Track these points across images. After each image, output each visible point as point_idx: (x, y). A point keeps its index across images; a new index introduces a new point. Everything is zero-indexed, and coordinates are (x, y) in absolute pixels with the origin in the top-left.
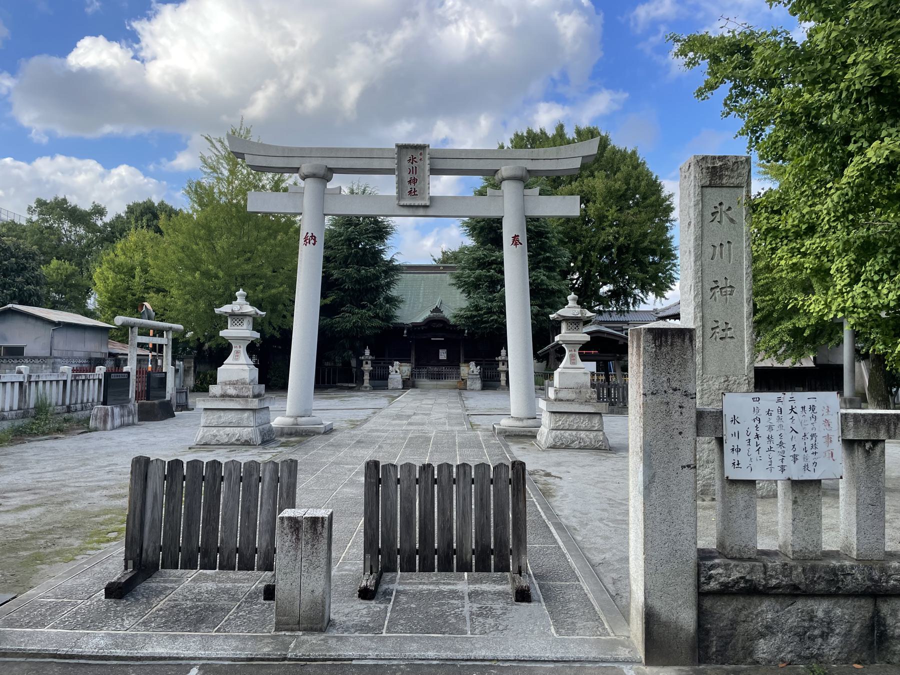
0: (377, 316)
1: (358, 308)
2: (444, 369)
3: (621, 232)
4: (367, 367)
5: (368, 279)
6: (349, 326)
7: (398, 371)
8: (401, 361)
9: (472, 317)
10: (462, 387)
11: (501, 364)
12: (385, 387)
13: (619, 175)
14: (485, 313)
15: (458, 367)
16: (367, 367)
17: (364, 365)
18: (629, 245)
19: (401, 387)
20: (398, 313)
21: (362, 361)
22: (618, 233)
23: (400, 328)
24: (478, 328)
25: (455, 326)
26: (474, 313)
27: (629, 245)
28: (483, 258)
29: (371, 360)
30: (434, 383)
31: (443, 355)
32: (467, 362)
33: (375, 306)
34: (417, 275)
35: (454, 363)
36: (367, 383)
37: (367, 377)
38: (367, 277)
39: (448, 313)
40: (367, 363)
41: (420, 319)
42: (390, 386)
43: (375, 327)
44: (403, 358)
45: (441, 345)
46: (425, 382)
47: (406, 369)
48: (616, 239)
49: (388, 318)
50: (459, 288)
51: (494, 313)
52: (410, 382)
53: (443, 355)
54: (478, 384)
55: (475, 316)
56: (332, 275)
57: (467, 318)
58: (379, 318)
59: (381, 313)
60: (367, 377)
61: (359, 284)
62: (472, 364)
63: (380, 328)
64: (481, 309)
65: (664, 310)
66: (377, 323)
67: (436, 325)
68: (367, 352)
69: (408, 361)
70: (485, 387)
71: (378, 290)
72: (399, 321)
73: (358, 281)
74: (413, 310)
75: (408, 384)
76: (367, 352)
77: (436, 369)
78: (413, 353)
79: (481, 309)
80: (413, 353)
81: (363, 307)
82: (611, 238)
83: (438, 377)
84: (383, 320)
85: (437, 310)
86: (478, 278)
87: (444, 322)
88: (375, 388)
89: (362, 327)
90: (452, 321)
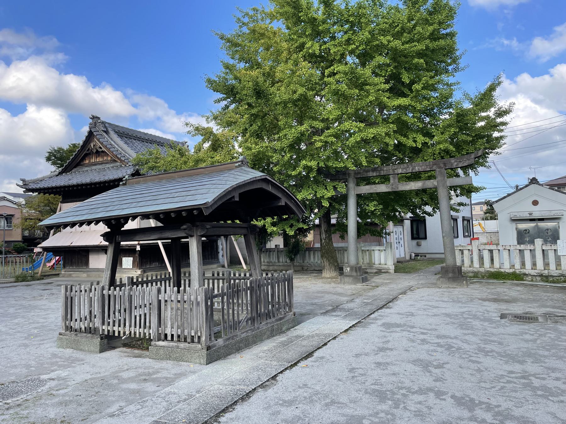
65: (34, 182)
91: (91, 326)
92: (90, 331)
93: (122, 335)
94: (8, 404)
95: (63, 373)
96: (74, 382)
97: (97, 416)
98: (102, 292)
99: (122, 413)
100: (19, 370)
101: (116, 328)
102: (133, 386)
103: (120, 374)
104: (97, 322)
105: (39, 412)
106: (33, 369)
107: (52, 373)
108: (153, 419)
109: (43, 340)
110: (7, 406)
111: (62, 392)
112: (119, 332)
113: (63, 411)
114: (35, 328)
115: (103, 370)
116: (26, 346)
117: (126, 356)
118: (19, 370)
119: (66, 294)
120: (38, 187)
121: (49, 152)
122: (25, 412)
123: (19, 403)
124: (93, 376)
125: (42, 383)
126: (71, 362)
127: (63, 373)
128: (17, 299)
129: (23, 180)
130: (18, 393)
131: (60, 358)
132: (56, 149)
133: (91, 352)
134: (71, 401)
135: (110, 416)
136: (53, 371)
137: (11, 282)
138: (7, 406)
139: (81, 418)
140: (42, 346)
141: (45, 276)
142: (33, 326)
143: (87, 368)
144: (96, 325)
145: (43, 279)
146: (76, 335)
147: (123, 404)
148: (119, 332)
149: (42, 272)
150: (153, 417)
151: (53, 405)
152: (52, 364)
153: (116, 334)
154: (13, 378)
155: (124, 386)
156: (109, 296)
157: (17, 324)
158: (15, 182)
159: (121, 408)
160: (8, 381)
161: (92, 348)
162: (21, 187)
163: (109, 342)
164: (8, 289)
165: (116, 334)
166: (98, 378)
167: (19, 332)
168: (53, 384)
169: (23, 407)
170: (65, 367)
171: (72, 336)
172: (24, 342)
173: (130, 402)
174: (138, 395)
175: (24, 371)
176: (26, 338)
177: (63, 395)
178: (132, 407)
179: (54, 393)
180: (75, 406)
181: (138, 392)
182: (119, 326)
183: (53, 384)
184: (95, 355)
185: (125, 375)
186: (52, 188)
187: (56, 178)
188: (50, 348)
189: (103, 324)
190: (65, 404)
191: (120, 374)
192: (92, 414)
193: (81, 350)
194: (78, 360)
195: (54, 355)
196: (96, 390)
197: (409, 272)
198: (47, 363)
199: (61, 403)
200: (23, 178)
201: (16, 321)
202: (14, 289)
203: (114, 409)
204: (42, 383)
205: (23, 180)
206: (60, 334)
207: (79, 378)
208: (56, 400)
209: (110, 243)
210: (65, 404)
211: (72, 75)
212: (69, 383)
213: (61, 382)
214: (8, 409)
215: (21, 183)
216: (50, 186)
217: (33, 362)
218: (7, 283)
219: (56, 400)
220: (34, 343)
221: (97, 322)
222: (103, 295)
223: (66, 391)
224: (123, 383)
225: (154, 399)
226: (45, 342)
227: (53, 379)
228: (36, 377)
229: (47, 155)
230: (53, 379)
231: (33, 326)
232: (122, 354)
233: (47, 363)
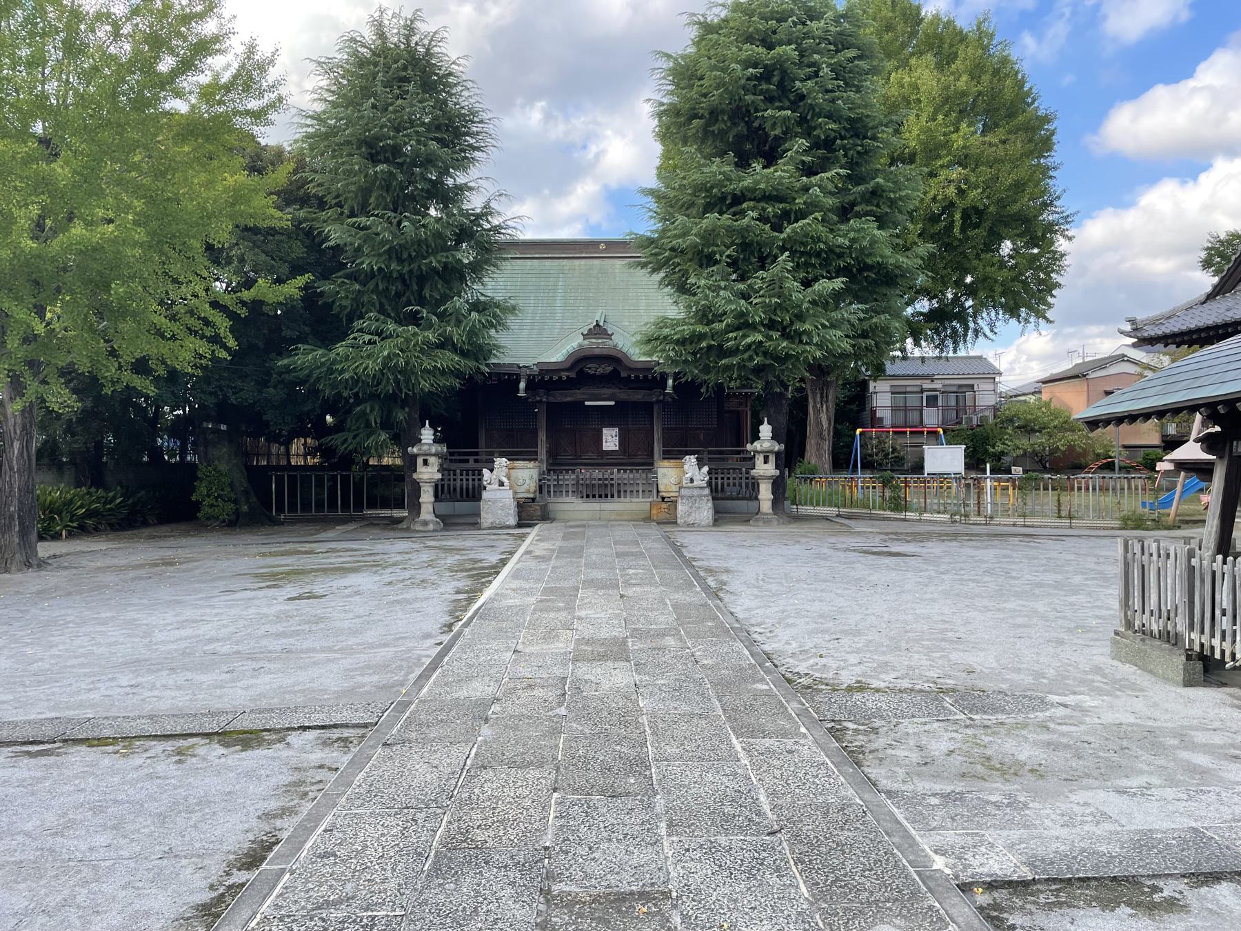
0: (445, 343)
1: (399, 322)
2: (616, 474)
3: (973, 179)
4: (428, 473)
5: (422, 247)
6: (373, 366)
7: (506, 481)
8: (512, 456)
9: (696, 338)
10: (663, 516)
11: (759, 460)
12: (472, 522)
13: (958, 65)
14: (731, 328)
15: (648, 464)
16: (428, 473)
17: (420, 467)
18: (986, 207)
19: (512, 521)
20: (498, 337)
21: (415, 456)
22: (967, 181)
23: (506, 380)
24: (707, 370)
25: (647, 369)
26: (700, 329)
27: (986, 207)
28: (720, 184)
29: (778, 454)
30: (594, 506)
31: (610, 440)
32: (674, 452)
33: (441, 317)
34: (548, 263)
35: (637, 457)
36: (427, 513)
37: (427, 497)
38: (419, 242)
39: (629, 342)
40: (425, 462)
41: (557, 354)
42: (487, 518)
43: (443, 372)
44: (519, 449)
45: (608, 417)
46: (571, 506)
47: (526, 475)
48: (961, 192)
49: (477, 351)
50: (654, 270)
51: (753, 327)
52: (536, 509)
53: (610, 440)
54: (705, 511)
55: (702, 337)
56: (327, 239)
57: (682, 342)
58: (454, 349)
59: (457, 334)
60: (427, 497)
61: (400, 261)
62: (691, 460)
63: (458, 374)
64: (719, 317)
65: (1155, 322)
66: (447, 359)
67: (596, 369)
68: (427, 435)
69: (531, 456)
70: (721, 516)
71: (454, 276)
72: (507, 360)
73: (394, 253)
74: (538, 334)
75: (530, 513)
76: (427, 435)
77: (597, 473)
78: (542, 437)
79: (719, 317)
80: (542, 437)
81: (414, 319)
82: (952, 190)
83: (601, 492)
84: (464, 354)
85: (598, 331)
86: (709, 236)
87: (615, 360)
88: (448, 522)
89: (407, 371)
90: (637, 354)
91: (1169, 628)
92: (1170, 638)
93: (1227, 659)
94: (972, 720)
95: (1088, 701)
96: (1097, 721)
97: (1096, 783)
98: (1189, 561)
99: (1143, 795)
100: (1022, 676)
101: (1216, 642)
102: (1201, 760)
103: (1193, 733)
104: (1181, 624)
105: (1007, 745)
106: (1045, 681)
107: (1072, 697)
108: (1194, 825)
109: (1097, 640)
110: (968, 722)
111: (1064, 728)
112: (1223, 652)
113: (1042, 756)
114: (1098, 617)
115: (1168, 717)
116: (1060, 642)
117: (1233, 706)
118: (1022, 676)
119: (1125, 558)
120: (1160, 333)
121: (1208, 249)
122: (987, 739)
123: (987, 723)
124: (1139, 721)
125: (1044, 704)
126: (1121, 686)
127: (1088, 701)
128: (1102, 560)
129: (1132, 321)
130: (995, 710)
131: (1104, 676)
132: (1222, 237)
133: (1167, 680)
134: (1067, 746)
135: (1118, 792)
136: (1075, 693)
137: (1113, 528)
138: (968, 722)
139: (1064, 776)
140: (1087, 650)
141: (1187, 522)
142: (1097, 612)
143: (1139, 705)
144: (1179, 628)
145: (1179, 527)
146: (1143, 640)
147: (1155, 781)
148: (1223, 652)
149: (1176, 515)
150: (1196, 820)
151: (1035, 743)
152: (1082, 682)
153: (1217, 656)
154: (1004, 686)
155: (1185, 755)
156: (1214, 573)
157: (1071, 604)
158: (1113, 328)
159: (1149, 786)
160: (996, 688)
161: (1171, 675)
162: (1128, 335)
163: (1208, 669)
164: (1098, 540)
165: (1217, 656)
166: (1145, 727)
167: (1065, 618)
168: (1060, 712)
169: (989, 731)
170: (1100, 692)
171: (1136, 642)
172: (1061, 636)
173: (1172, 782)
174: (1198, 776)
175: (1029, 680)
176: (1070, 630)
177: (1063, 734)
178: (1169, 793)
179: (1052, 726)
180: (1069, 756)
181: (1203, 772)
182: (1223, 638)
183: (1060, 712)
184: (1173, 689)
185: (1200, 737)
186: (1190, 332)
187: (1201, 308)
188: (1101, 655)
189: (1191, 627)
190: (1054, 746)
191: (1193, 733)
192: (1088, 776)
193: (1151, 672)
194: (1134, 687)
195: (1098, 670)
196: (1125, 743)
197: (746, 521)
198: (1075, 679)
199: (1049, 744)
200: (1130, 316)
201: (1072, 599)
202: (1107, 541)
203: (1134, 782)
204: (1044, 704)
205: (1132, 321)
206: (1117, 633)
207: (1109, 717)
208: (1045, 737)
209: (1221, 457)
210: (1054, 746)
211: (1202, 66)
212: (1088, 719)
213: (1075, 714)
214: (967, 727)
215: (1128, 328)
216: (1184, 328)
217: (1052, 671)
218: (1104, 529)
219: (1045, 737)
220: (1076, 641)
221: (1181, 624)
222: (1191, 570)
223: (1073, 728)
224: (1186, 748)
225: (1224, 794)
226: (1098, 643)
227: (1066, 706)
228: (1040, 695)
229: (1203, 255)
230: (1066, 706)
231: (1097, 612)
232: (1230, 700)
233: (1075, 679)
